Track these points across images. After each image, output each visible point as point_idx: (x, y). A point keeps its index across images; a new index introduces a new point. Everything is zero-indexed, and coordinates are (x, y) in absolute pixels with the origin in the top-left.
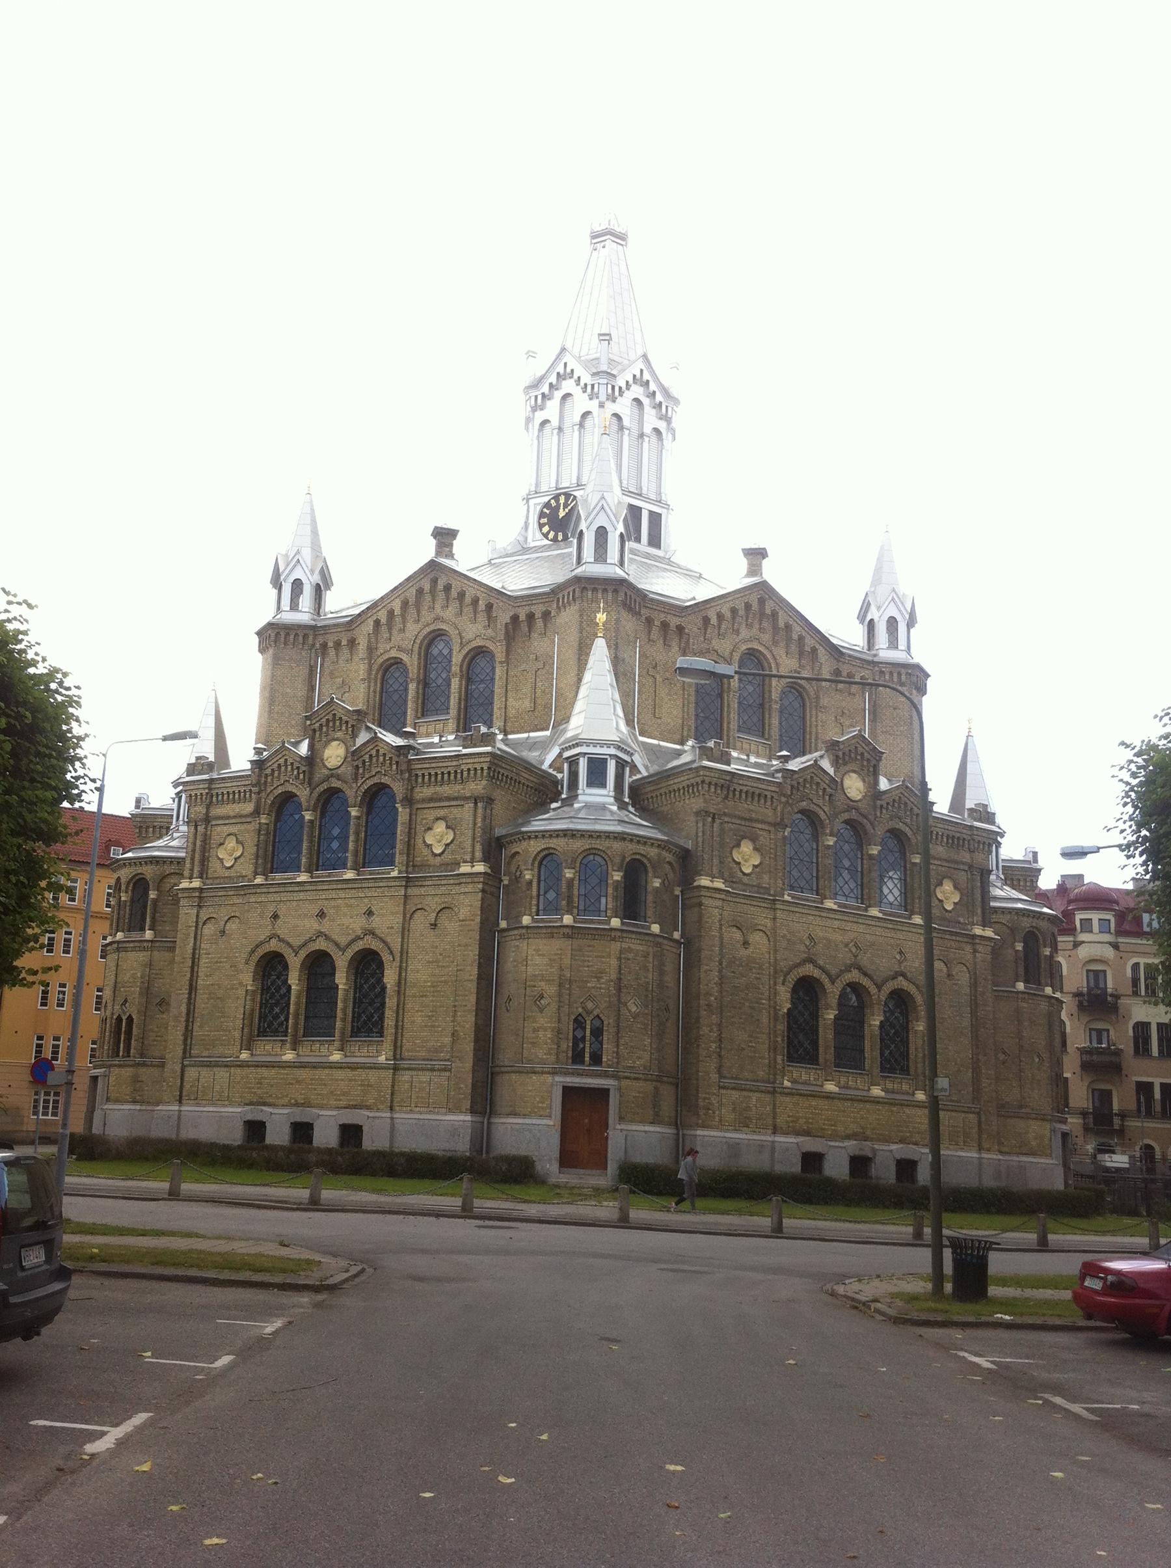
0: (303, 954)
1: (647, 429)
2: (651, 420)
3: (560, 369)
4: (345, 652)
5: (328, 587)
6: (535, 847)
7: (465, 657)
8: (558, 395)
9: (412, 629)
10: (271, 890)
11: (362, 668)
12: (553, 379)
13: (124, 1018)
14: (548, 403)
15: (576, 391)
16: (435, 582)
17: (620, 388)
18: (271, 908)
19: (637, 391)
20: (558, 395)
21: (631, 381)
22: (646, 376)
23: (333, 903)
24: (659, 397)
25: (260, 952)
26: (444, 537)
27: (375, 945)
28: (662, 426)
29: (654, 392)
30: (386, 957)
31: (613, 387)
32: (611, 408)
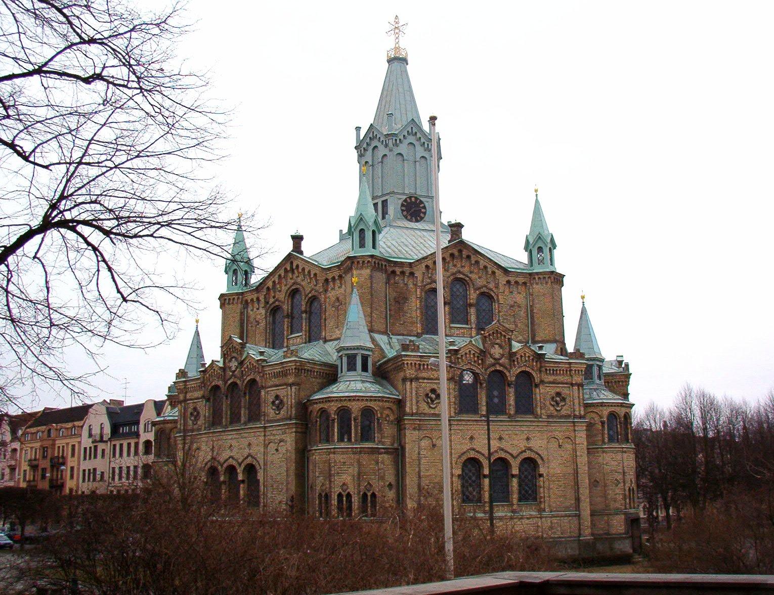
0: (519, 459)
1: (418, 159)
2: (420, 151)
3: (371, 135)
4: (256, 305)
5: (555, 248)
6: (317, 407)
7: (307, 302)
8: (371, 148)
9: (284, 288)
10: (468, 423)
11: (263, 311)
12: (368, 140)
13: (369, 494)
14: (368, 153)
15: (379, 144)
16: (292, 263)
17: (400, 140)
18: (470, 434)
19: (411, 139)
20: (371, 148)
21: (406, 134)
22: (415, 130)
23: (506, 432)
24: (423, 140)
25: (464, 458)
26: (297, 240)
27: (533, 455)
28: (426, 155)
29: (420, 138)
30: (257, 467)
31: (396, 140)
32: (397, 150)
